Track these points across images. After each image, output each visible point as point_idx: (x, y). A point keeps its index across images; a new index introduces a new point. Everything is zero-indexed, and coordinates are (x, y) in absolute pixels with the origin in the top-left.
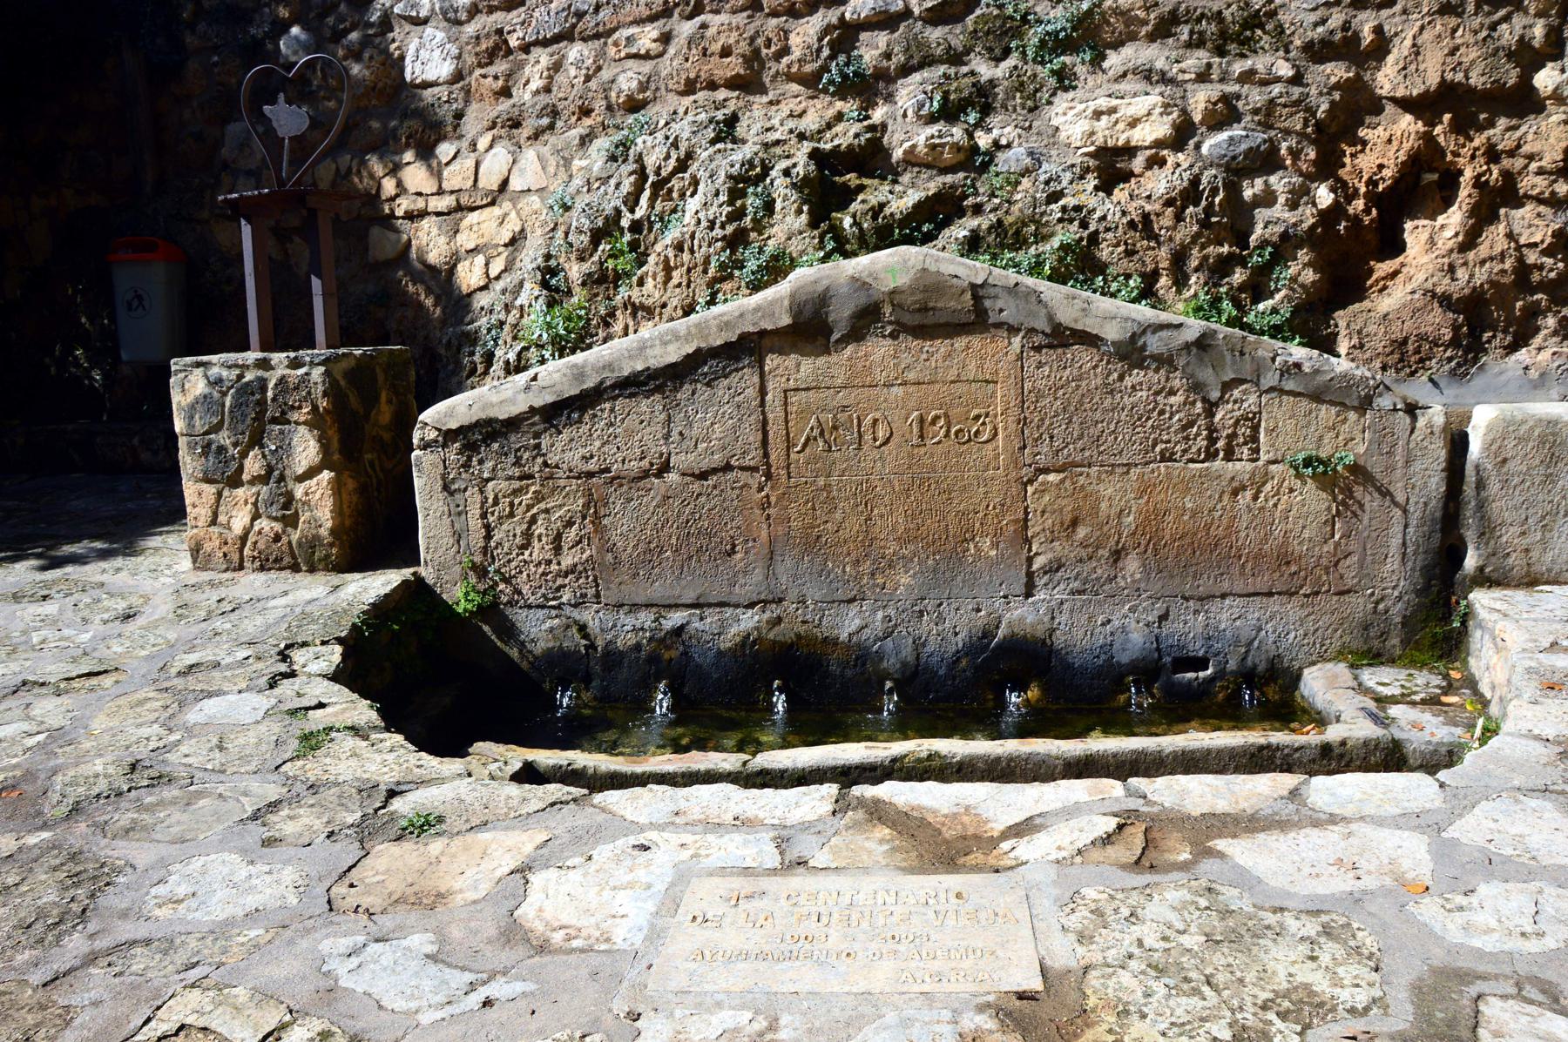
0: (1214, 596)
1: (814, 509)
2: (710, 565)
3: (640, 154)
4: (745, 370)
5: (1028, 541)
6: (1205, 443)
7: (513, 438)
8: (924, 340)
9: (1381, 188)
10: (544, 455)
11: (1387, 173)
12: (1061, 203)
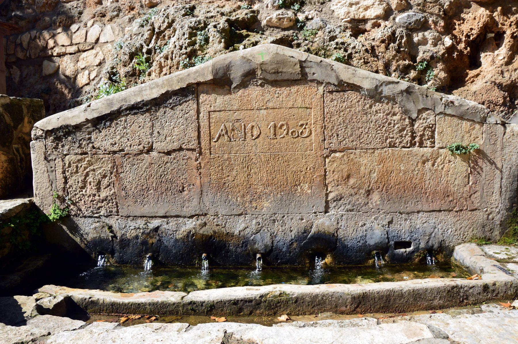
0: (414, 212)
1: (222, 170)
2: (172, 197)
3: (153, 23)
4: (190, 102)
5: (326, 186)
6: (410, 138)
7: (78, 134)
8: (277, 87)
9: (471, 38)
10: (93, 143)
11: (474, 32)
12: (336, 41)
